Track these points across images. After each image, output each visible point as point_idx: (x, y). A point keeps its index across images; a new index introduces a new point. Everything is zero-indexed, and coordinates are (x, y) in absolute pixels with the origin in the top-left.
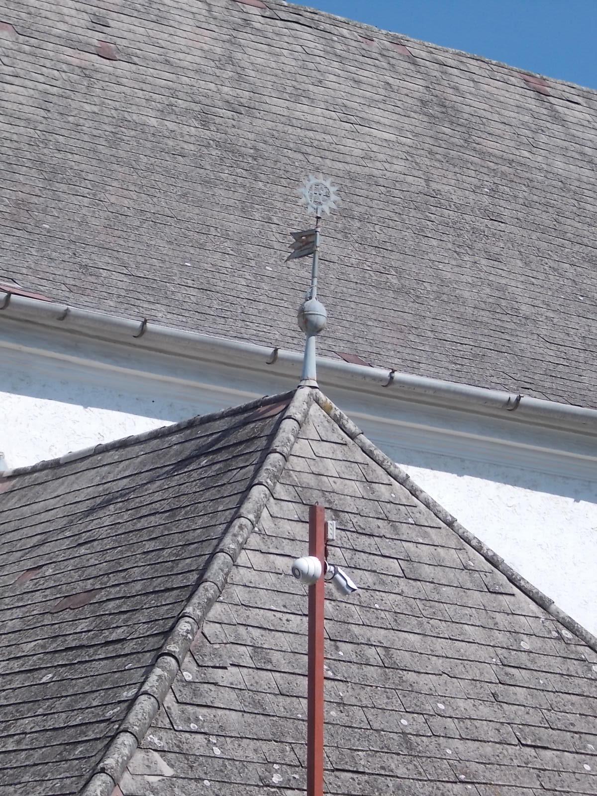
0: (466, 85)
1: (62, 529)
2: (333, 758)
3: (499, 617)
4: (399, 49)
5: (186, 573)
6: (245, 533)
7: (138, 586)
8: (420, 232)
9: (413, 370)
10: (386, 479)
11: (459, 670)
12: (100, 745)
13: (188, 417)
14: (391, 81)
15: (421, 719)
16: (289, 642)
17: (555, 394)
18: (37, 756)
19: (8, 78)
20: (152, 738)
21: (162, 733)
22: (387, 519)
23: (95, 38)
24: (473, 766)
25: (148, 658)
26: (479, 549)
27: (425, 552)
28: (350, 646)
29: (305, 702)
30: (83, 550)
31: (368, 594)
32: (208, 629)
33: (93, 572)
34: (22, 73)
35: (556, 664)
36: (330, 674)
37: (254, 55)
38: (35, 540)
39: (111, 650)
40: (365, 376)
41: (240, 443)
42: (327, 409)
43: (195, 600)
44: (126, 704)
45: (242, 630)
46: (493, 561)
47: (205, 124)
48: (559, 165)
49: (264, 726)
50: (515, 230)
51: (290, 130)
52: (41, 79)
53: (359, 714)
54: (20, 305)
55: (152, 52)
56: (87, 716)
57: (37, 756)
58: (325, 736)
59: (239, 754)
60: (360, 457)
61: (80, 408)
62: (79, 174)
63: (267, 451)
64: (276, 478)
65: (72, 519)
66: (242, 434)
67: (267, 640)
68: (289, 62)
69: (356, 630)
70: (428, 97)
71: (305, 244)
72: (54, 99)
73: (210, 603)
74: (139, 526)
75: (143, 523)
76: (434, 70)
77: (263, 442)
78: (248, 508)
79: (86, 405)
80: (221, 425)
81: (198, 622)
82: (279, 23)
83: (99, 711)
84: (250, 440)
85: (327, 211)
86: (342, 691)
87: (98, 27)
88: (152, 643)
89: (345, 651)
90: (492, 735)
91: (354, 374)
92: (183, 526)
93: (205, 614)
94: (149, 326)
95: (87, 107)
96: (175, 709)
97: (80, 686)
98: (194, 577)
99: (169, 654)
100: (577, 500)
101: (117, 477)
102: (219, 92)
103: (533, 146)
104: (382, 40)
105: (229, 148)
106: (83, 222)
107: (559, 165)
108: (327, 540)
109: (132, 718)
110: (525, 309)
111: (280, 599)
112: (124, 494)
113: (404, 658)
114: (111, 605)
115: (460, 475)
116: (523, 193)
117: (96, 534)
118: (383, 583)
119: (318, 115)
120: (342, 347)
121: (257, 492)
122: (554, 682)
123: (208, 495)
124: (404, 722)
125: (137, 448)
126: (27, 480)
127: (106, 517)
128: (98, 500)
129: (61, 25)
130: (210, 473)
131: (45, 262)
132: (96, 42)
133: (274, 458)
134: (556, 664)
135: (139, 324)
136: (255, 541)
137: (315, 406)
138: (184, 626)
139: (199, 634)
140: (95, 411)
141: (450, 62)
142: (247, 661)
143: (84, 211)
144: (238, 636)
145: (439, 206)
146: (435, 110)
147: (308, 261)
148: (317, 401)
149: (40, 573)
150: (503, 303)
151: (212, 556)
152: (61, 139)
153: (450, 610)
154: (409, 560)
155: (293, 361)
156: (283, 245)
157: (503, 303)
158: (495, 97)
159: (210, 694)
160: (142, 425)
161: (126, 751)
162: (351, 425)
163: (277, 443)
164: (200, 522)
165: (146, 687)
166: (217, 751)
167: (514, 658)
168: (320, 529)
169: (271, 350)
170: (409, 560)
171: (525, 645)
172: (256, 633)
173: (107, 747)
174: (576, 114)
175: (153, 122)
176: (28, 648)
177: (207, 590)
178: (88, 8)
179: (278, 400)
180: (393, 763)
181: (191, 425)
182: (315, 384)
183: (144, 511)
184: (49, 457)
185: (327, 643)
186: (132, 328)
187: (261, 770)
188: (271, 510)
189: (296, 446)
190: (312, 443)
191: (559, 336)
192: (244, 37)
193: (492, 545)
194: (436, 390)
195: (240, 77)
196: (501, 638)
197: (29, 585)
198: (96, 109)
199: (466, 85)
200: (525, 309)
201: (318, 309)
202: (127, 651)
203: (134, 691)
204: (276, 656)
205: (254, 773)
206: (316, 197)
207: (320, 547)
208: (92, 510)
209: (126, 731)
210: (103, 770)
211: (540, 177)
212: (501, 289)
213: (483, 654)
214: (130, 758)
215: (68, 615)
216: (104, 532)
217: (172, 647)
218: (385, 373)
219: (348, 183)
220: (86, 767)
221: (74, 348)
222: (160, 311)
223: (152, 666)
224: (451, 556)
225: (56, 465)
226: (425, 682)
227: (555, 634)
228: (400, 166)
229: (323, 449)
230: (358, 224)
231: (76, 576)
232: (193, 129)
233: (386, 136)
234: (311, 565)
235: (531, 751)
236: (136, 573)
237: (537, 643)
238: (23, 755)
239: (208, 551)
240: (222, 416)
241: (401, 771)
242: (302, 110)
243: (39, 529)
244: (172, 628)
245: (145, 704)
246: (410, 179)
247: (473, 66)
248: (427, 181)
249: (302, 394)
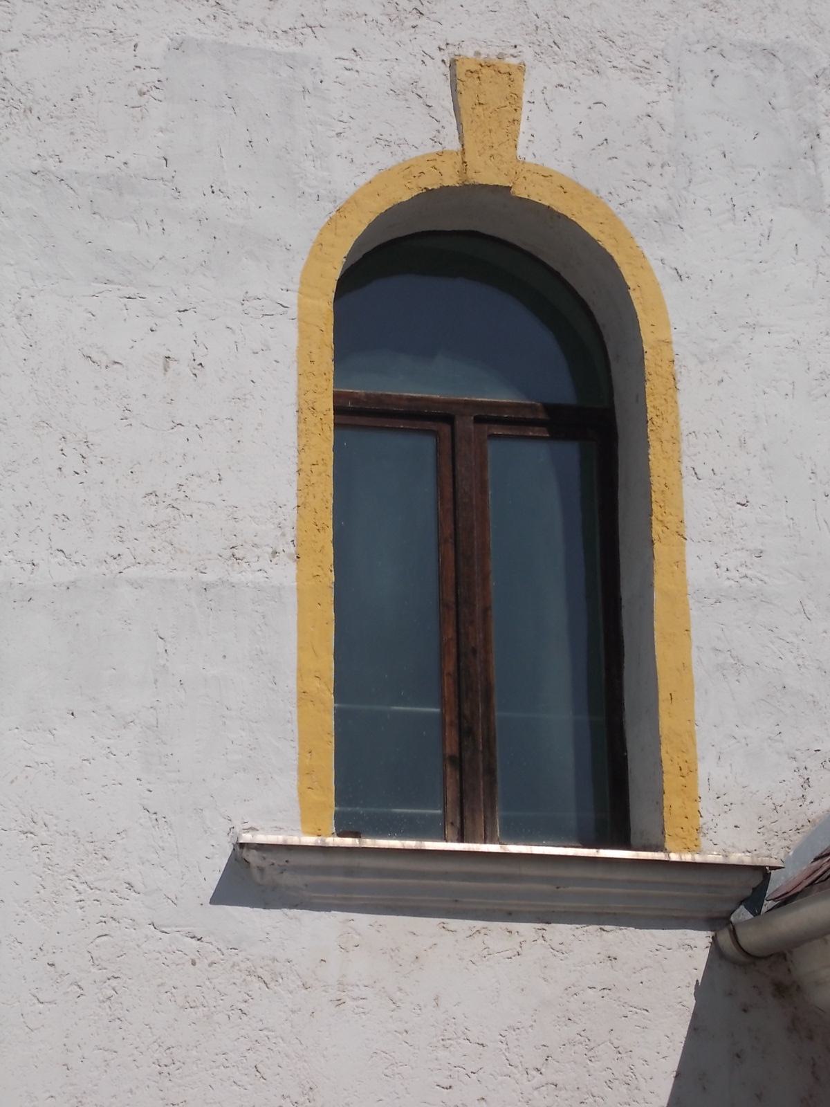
47: (225, 723)
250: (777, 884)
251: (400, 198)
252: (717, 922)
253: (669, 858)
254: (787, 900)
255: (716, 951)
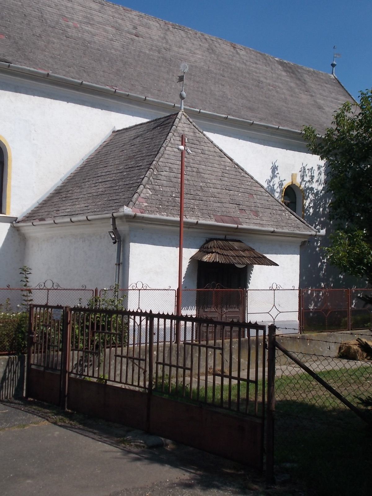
0: (217, 45)
1: (128, 143)
2: (186, 191)
3: (222, 162)
4: (203, 36)
5: (154, 151)
6: (168, 143)
7: (145, 154)
8: (207, 79)
9: (204, 110)
10: (198, 132)
11: (213, 174)
12: (136, 187)
13: (155, 119)
14: (201, 44)
15: (205, 183)
16: (177, 167)
17: (236, 116)
18: (123, 190)
19: (115, 40)
20: (147, 186)
21: (150, 185)
22: (199, 141)
23: (134, 31)
24: (216, 194)
25: (147, 169)
26: (218, 148)
27: (206, 148)
28: (190, 168)
29: (180, 179)
30: (132, 147)
31: (194, 157)
32: (160, 163)
33: (135, 151)
34: (118, 39)
35: (234, 173)
36: (186, 174)
37: (170, 37)
38: (122, 145)
39: (139, 168)
40: (194, 111)
41: (167, 124)
42: (186, 117)
43: (157, 157)
44: (142, 179)
45: (167, 163)
46: (221, 151)
47: (159, 53)
48: (238, 64)
49: (171, 184)
50: (228, 79)
51: (178, 55)
52: (122, 41)
53: (191, 182)
54: (118, 93)
55: (147, 35)
56: (134, 182)
57: (123, 190)
58: (185, 187)
59: (166, 190)
60: (193, 127)
61: (131, 117)
62: (131, 64)
63: (173, 125)
64: (174, 131)
65: (130, 140)
66: (167, 122)
67: (172, 166)
68: (179, 40)
69: (191, 164)
70: (209, 48)
71: (181, 79)
72: (125, 46)
73: (160, 158)
74: (145, 142)
75: (146, 141)
76: (211, 42)
77: (171, 124)
78: (168, 137)
79: (133, 116)
80: (162, 120)
81: (157, 162)
82: (176, 29)
83: (136, 180)
84: (169, 123)
85: (186, 71)
86: (188, 177)
87: (135, 29)
88: (148, 166)
89: (189, 169)
90: (220, 187)
91: (192, 110)
92: (154, 141)
93: (159, 160)
94: (147, 98)
95: (132, 48)
96: (152, 180)
97: (132, 175)
98: (157, 152)
99: (151, 168)
100: (239, 139)
101: (140, 131)
102: (162, 45)
103: (232, 60)
104: (199, 34)
105: (165, 59)
106: (132, 75)
107: (238, 64)
108: (185, 142)
109: (143, 182)
110: (229, 97)
111: (175, 157)
112: (141, 135)
113: (201, 171)
114: (139, 158)
115: (214, 133)
116: (230, 70)
117: (135, 144)
118: (197, 154)
119: (185, 51)
120: (189, 104)
121: (170, 134)
122: (233, 177)
123: (160, 135)
124: (201, 184)
125: (144, 125)
126: (120, 132)
127: (138, 140)
128: (136, 136)
129: (127, 28)
130: (160, 130)
131: (124, 83)
132: (134, 32)
133: (174, 127)
134: (234, 173)
135: (145, 98)
136: (170, 145)
137: (183, 116)
138: (154, 163)
139: (157, 165)
140: (135, 117)
141: (214, 40)
142: (168, 171)
143: (132, 72)
144: (166, 165)
145: (211, 73)
146: (211, 51)
147: (182, 82)
148: (184, 115)
149: (123, 152)
150: (225, 96)
151: (161, 148)
152: (127, 55)
153: (211, 161)
154: (203, 150)
155: (178, 107)
156: (176, 79)
157: (225, 96)
158: (224, 48)
159: (160, 177)
160: (145, 120)
161: (142, 189)
162: (191, 120)
163: (175, 124)
164: (158, 141)
165: (146, 175)
166: (161, 189)
167: (225, 171)
168: (184, 140)
169: (174, 104)
170: (203, 150)
171: (227, 169)
172: (170, 164)
173: (138, 188)
174: (242, 52)
175: (148, 52)
176: (121, 167)
177: (159, 155)
178: (132, 24)
179: (175, 115)
180: (199, 193)
181: (156, 120)
182: (183, 111)
183: (146, 139)
184: (125, 127)
185: (185, 167)
186: (143, 99)
187: (171, 193)
188: (173, 138)
189: (179, 125)
190: (182, 124)
191: (237, 103)
192: (168, 33)
193: (221, 147)
194: (210, 114)
195: (167, 42)
196: (222, 167)
197: (121, 155)
198: (135, 48)
199: (217, 45)
200: (229, 97)
201: (184, 94)
202: (142, 168)
203: (143, 176)
204: (174, 169)
205: (169, 194)
206: (184, 67)
207: (184, 144)
208: (134, 139)
209: (142, 184)
210: (137, 193)
211: (233, 67)
212: (224, 92)
213: (218, 170)
214: (143, 190)
215: (129, 161)
216: (137, 143)
217: (152, 167)
218: (198, 110)
219: (191, 67)
220: (133, 192)
221: (130, 103)
222: (149, 95)
223: (148, 171)
224: (212, 149)
225: (126, 129)
226: (206, 176)
227: (234, 166)
228: (202, 64)
229: (185, 125)
230: (193, 77)
231: (131, 152)
232: (156, 54)
233: (199, 57)
234: (182, 147)
235: (228, 191)
236: (144, 152)
237: (230, 168)
238: (120, 190)
239: (160, 147)
240: (163, 118)
241: (200, 194)
242: (181, 50)
243: (123, 143)
244: (152, 163)
245: (146, 179)
246: (205, 67)
247: (219, 41)
248: (209, 67)
249: (180, 113)
250: (18, 220)
251: (177, 257)
252: (12, 223)
253: (121, 288)
254: (18, 222)
255: (11, 226)
